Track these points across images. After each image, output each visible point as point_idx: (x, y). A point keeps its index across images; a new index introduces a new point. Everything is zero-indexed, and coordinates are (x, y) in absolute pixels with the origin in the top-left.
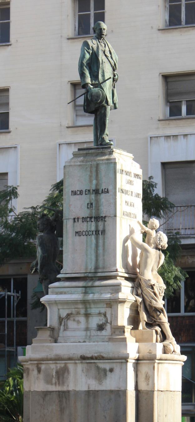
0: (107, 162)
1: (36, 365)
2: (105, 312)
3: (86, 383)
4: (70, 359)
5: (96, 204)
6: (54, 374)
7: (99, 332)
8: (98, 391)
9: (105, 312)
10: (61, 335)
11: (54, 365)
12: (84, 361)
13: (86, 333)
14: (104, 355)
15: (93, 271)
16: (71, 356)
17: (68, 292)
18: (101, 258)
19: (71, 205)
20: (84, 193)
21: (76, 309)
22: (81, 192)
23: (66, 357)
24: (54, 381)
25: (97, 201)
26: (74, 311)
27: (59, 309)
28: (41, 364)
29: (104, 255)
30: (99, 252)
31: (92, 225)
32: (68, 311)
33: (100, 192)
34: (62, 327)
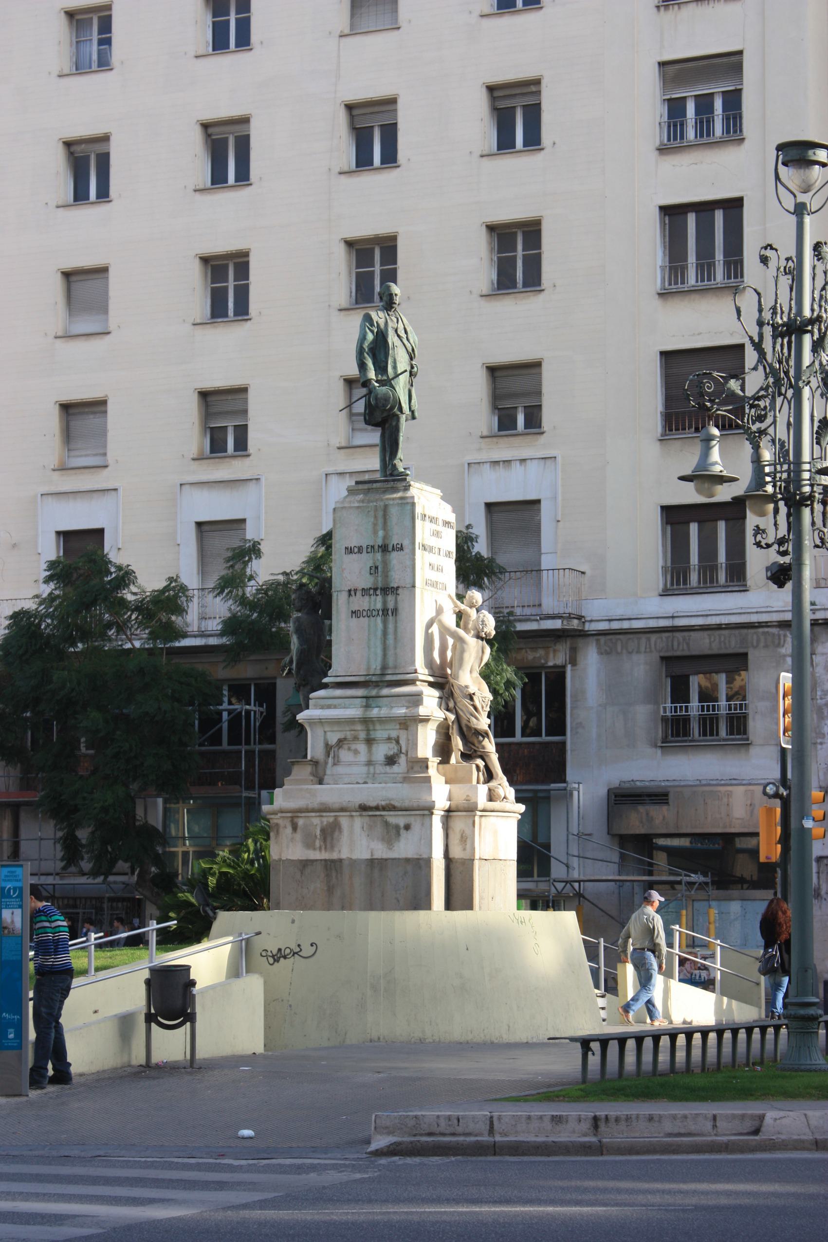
0: (400, 502)
1: (290, 819)
2: (398, 737)
3: (368, 847)
4: (342, 810)
5: (384, 567)
6: (318, 833)
7: (388, 767)
8: (386, 860)
9: (398, 737)
10: (328, 772)
11: (318, 819)
12: (364, 813)
13: (369, 770)
14: (397, 804)
15: (378, 672)
16: (345, 804)
17: (340, 705)
18: (391, 653)
19: (345, 569)
20: (365, 550)
21: (352, 732)
22: (360, 550)
23: (337, 806)
24: (318, 843)
25: (385, 563)
26: (349, 735)
27: (325, 732)
28: (298, 817)
29: (395, 648)
30: (387, 642)
31: (378, 601)
32: (339, 735)
33: (390, 549)
34: (330, 760)
